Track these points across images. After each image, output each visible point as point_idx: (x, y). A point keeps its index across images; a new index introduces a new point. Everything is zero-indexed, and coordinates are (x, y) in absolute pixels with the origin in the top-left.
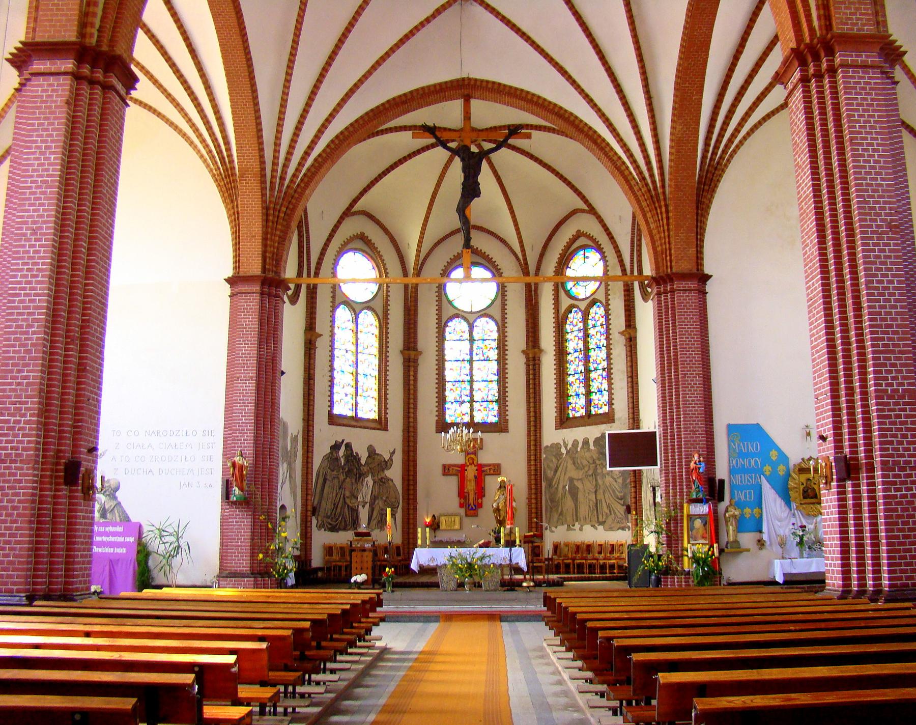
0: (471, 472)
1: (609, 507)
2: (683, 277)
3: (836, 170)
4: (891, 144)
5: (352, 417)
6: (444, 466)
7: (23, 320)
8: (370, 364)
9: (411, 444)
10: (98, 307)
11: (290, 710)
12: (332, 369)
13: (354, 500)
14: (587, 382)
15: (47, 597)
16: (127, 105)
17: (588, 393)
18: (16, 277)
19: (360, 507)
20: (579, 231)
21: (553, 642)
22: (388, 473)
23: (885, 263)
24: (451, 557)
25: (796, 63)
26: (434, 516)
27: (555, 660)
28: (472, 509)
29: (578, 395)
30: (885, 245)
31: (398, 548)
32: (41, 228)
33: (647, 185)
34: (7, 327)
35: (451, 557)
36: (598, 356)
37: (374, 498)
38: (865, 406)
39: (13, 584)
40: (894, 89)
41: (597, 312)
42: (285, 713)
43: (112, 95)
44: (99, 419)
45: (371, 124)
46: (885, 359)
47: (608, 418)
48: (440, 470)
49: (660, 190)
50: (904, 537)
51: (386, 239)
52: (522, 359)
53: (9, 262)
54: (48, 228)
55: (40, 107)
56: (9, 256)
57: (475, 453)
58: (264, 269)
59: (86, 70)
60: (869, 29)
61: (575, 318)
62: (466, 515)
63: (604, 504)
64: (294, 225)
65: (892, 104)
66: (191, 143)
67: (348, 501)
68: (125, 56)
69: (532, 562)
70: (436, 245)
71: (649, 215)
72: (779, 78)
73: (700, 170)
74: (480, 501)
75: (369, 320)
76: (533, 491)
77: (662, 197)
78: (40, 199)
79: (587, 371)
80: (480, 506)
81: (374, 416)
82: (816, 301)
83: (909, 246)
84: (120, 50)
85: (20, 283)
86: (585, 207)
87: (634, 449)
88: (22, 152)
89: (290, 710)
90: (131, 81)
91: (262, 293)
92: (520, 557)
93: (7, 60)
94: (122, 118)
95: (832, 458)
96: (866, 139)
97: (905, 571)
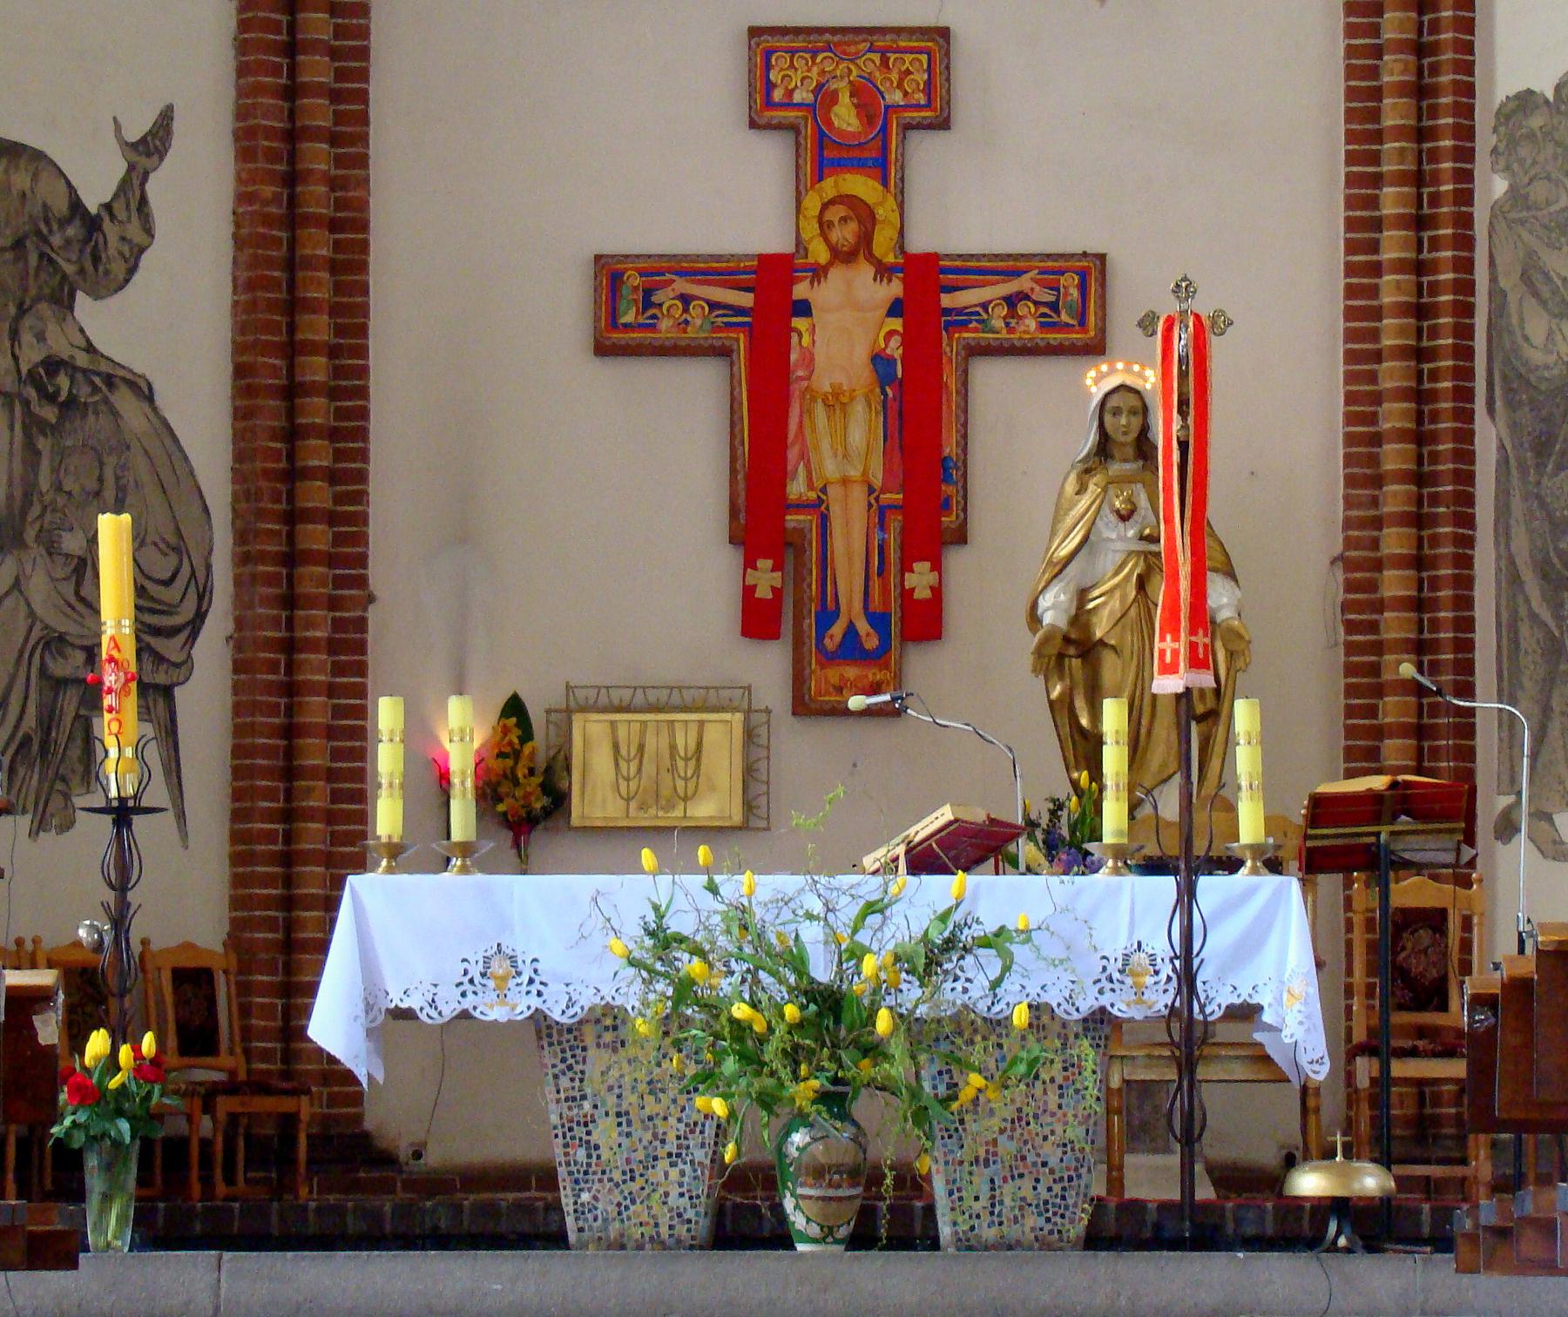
0: (845, 328)
6: (610, 274)
9: (317, 70)
22: (109, 325)
24: (664, 940)
26: (514, 708)
28: (851, 648)
31: (193, 980)
35: (664, 940)
48: (570, 305)
57: (880, 161)
62: (803, 706)
69: (1375, 1046)
74: (920, 579)
76: (1395, 498)
80: (925, 621)
92: (1272, 953)
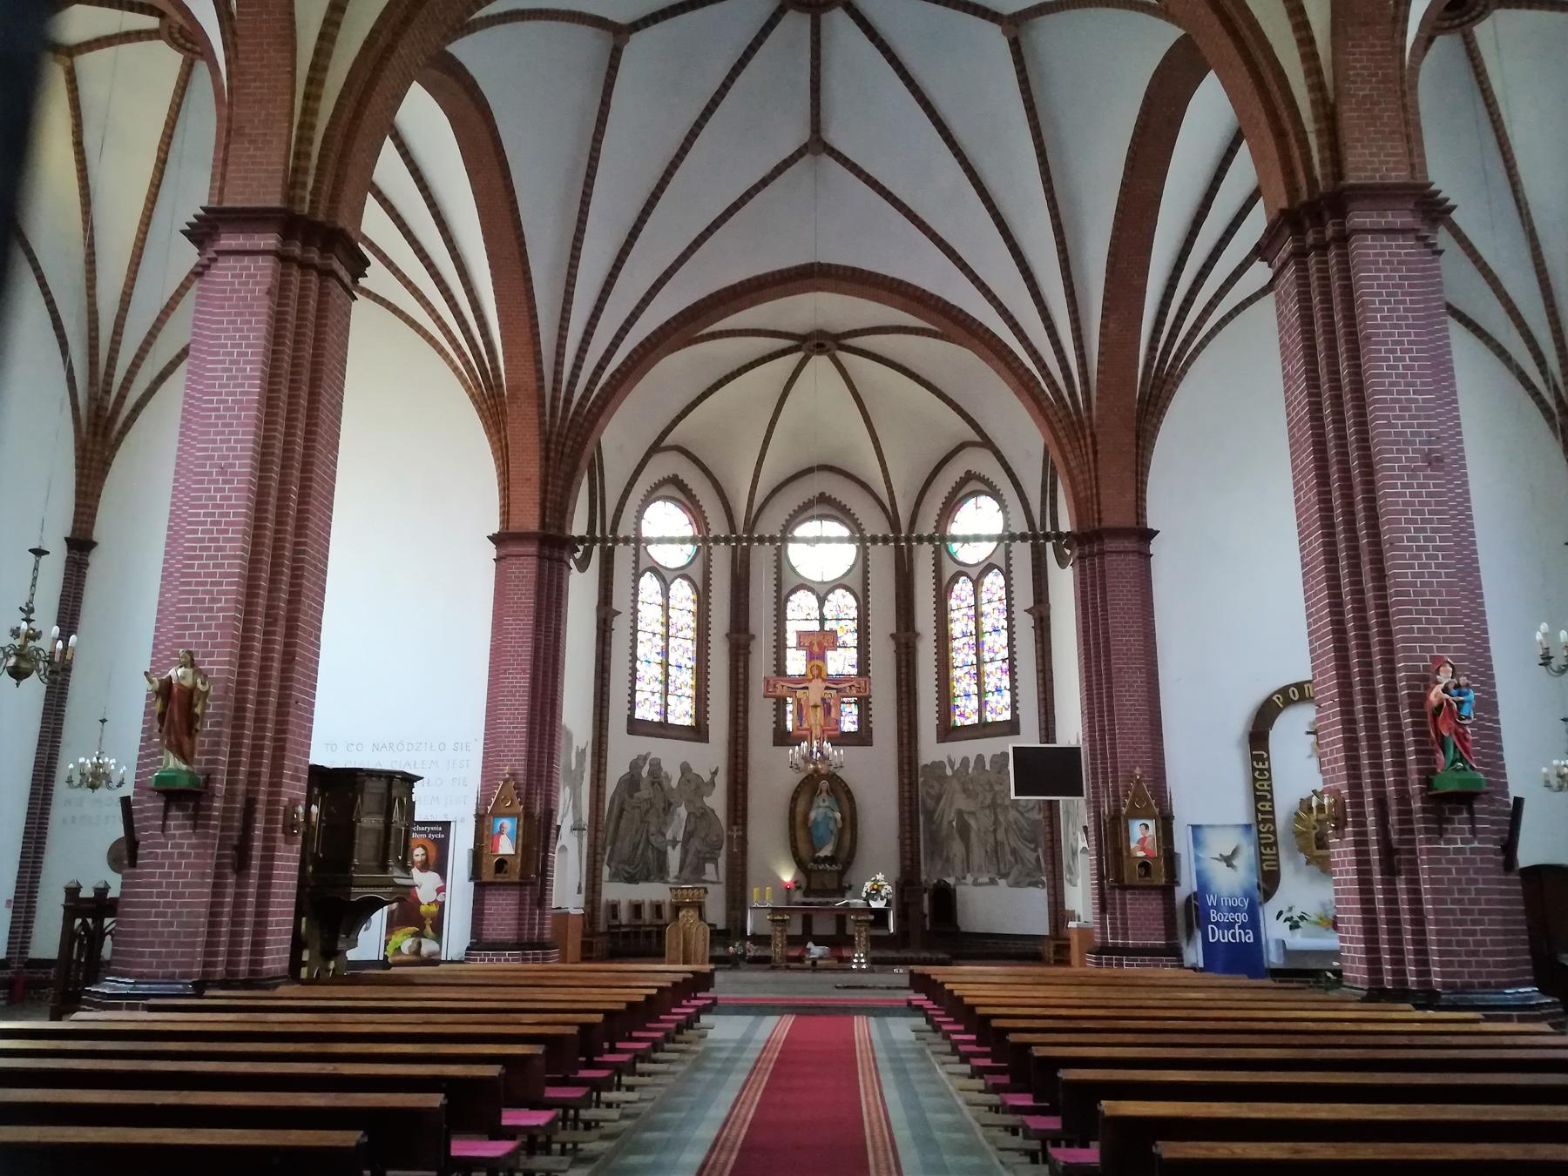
1: (1014, 852)
2: (1117, 533)
3: (1345, 381)
4: (1431, 341)
5: (660, 723)
7: (205, 592)
8: (683, 651)
10: (313, 574)
11: (569, 1146)
12: (634, 658)
13: (660, 839)
14: (979, 676)
15: (225, 984)
16: (355, 298)
17: (981, 694)
18: (196, 532)
19: (669, 848)
20: (968, 472)
21: (939, 1048)
23: (1421, 512)
25: (1287, 232)
27: (944, 1076)
29: (967, 695)
30: (1420, 486)
32: (232, 466)
33: (1065, 407)
34: (180, 601)
36: (996, 643)
37: (689, 835)
38: (1394, 718)
39: (176, 965)
40: (1433, 261)
41: (994, 581)
42: (563, 1152)
43: (333, 285)
44: (310, 729)
45: (686, 328)
46: (1423, 649)
47: (1012, 727)
49: (1084, 415)
50: (1463, 912)
51: (708, 483)
52: (891, 646)
53: (185, 512)
54: (243, 466)
55: (231, 299)
56: (186, 504)
58: (543, 524)
59: (296, 249)
60: (1399, 176)
61: (963, 588)
63: (1007, 849)
64: (584, 464)
65: (1433, 281)
66: (441, 351)
67: (652, 839)
68: (349, 229)
70: (775, 491)
71: (1068, 448)
72: (1261, 251)
73: (1142, 383)
75: (682, 593)
77: (1087, 423)
78: (231, 425)
79: (980, 663)
81: (688, 721)
82: (1315, 567)
83: (1458, 486)
84: (342, 223)
85: (202, 540)
86: (978, 439)
87: (1047, 770)
88: (204, 360)
89: (569, 1146)
90: (359, 266)
91: (540, 557)
93: (183, 232)
94: (348, 315)
95: (1345, 791)
96: (1392, 335)
97: (1468, 964)
